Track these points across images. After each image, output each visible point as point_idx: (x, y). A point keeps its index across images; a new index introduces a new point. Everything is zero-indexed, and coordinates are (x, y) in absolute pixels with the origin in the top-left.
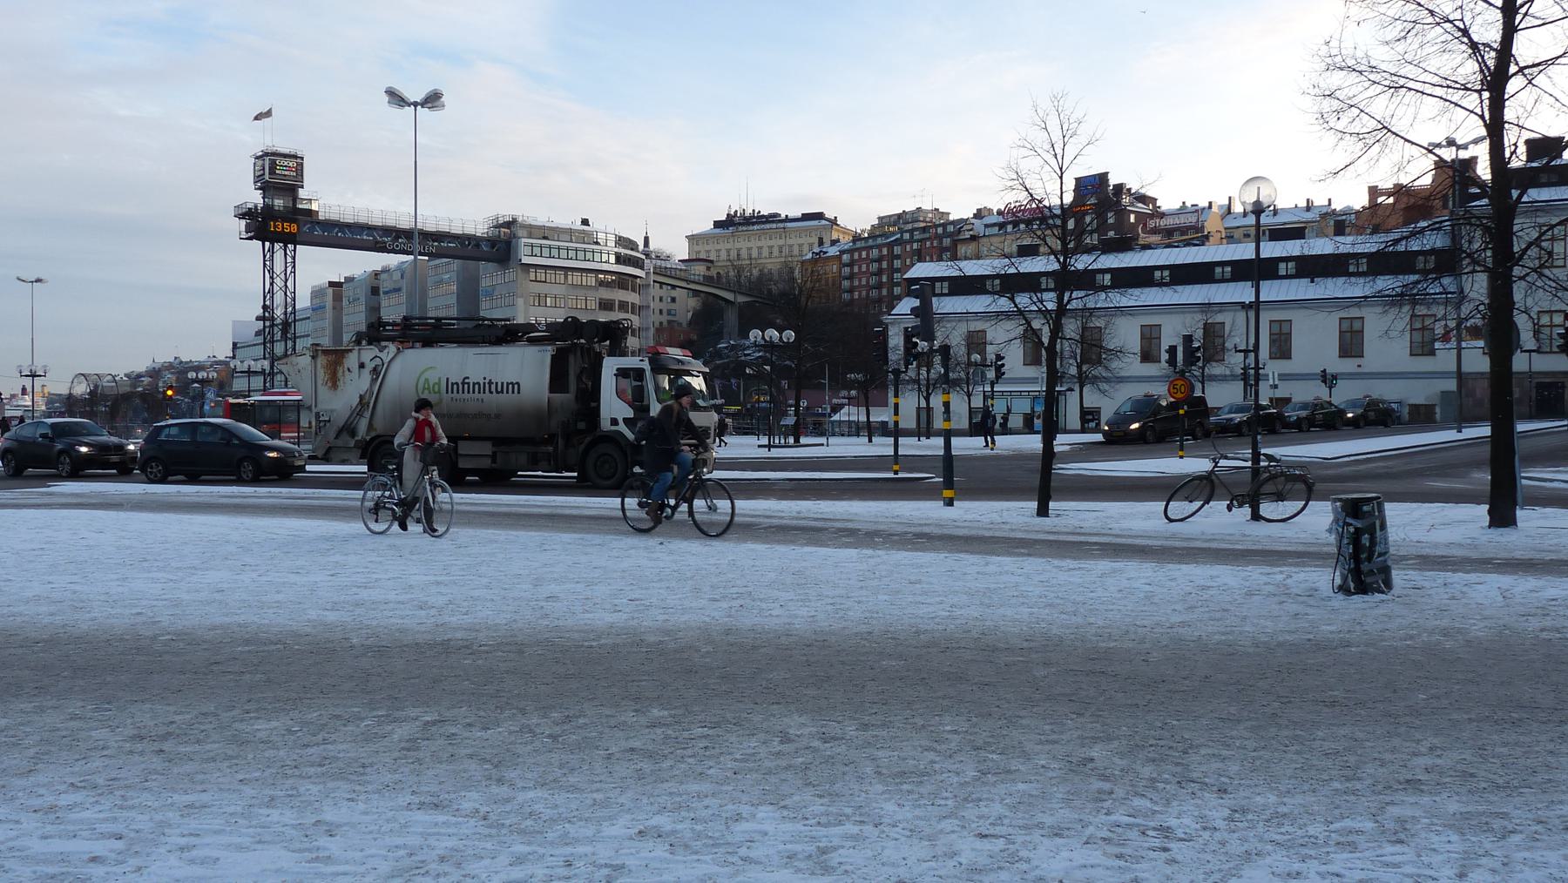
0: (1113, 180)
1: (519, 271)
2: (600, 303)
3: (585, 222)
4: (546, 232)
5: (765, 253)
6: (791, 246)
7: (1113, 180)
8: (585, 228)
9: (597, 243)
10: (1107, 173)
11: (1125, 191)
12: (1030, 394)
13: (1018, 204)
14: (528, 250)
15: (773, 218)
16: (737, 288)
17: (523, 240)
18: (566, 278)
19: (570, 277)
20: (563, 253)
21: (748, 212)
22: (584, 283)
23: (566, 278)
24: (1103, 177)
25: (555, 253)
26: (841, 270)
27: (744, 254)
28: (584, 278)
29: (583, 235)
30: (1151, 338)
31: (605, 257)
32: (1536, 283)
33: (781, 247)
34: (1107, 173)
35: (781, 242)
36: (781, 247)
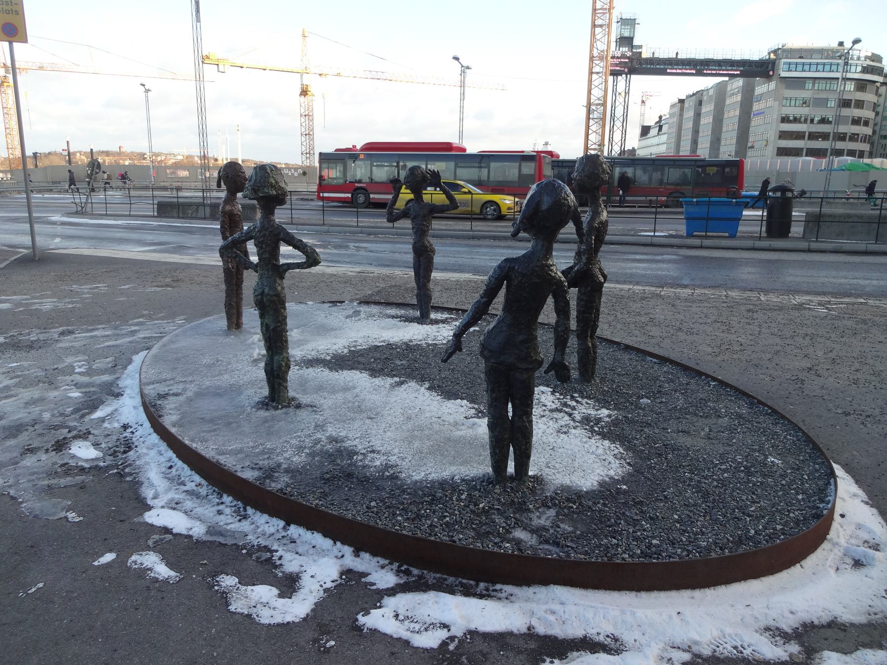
4: (802, 53)
18: (813, 85)
22: (828, 88)
23: (813, 85)
32: (810, 88)
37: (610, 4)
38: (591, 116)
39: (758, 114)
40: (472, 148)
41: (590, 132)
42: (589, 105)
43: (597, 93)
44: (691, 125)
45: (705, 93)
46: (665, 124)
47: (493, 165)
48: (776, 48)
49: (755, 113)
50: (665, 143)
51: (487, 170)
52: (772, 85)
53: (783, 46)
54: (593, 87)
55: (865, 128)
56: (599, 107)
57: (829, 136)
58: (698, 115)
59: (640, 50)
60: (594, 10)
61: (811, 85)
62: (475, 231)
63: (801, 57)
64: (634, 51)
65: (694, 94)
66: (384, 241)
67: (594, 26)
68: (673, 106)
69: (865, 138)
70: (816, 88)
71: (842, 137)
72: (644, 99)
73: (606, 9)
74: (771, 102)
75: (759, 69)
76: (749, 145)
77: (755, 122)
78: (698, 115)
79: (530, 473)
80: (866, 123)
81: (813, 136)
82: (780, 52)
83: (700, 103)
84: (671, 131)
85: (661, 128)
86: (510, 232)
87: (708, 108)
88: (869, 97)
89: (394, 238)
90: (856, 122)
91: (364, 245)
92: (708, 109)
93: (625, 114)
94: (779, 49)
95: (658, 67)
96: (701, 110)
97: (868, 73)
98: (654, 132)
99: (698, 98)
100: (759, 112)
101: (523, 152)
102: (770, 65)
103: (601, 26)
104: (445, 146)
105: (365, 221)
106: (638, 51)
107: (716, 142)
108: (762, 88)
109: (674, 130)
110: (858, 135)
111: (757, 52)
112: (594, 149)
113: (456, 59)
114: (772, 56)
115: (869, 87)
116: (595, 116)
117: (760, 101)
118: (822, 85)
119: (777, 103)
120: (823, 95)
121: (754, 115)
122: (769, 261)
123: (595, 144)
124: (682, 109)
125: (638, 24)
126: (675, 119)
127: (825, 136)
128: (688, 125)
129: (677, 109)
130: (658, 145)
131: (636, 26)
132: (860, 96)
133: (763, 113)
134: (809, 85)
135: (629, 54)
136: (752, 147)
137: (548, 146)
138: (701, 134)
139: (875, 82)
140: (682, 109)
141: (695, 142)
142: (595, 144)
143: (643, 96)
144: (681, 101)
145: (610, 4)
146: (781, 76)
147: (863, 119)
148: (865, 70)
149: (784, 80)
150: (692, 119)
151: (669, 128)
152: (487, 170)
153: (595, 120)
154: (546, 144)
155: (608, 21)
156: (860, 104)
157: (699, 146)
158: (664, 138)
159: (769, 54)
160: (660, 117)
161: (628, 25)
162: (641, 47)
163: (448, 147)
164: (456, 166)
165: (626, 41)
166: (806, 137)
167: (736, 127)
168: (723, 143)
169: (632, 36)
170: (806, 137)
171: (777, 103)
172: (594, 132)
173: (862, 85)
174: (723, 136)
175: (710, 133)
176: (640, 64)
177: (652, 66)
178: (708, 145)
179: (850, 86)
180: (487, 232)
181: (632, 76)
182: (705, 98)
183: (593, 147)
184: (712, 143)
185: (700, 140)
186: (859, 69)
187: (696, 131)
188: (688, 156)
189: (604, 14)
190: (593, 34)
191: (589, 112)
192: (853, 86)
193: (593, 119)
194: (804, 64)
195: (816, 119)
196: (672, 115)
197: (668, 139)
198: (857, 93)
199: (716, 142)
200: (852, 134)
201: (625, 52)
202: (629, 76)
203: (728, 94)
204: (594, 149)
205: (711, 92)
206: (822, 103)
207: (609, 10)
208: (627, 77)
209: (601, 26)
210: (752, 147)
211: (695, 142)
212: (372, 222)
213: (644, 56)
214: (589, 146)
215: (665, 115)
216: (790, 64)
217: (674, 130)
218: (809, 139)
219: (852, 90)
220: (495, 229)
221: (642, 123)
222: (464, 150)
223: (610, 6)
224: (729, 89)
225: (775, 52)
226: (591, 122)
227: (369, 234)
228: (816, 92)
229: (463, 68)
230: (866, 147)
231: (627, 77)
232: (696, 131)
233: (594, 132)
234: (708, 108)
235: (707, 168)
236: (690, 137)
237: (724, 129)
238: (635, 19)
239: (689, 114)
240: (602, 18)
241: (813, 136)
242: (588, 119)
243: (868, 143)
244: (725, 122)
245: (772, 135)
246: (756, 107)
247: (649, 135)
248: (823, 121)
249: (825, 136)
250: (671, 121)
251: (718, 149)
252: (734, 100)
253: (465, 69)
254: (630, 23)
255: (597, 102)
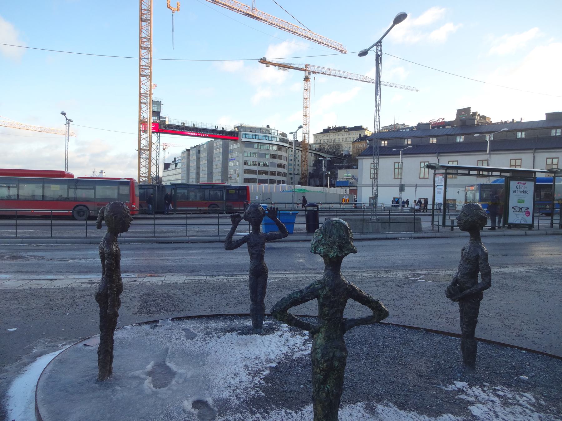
0: (472, 111)
1: (241, 144)
2: (271, 156)
3: (268, 126)
4: (251, 129)
5: (344, 140)
6: (350, 138)
7: (472, 111)
8: (268, 128)
9: (270, 134)
10: (470, 107)
11: (477, 115)
12: (503, 174)
13: (434, 121)
14: (244, 136)
15: (344, 128)
16: (328, 153)
17: (242, 132)
18: (258, 146)
19: (259, 146)
20: (257, 137)
21: (337, 126)
22: (265, 148)
23: (258, 146)
24: (468, 110)
25: (260, 137)
26: (366, 145)
27: (337, 140)
28: (265, 147)
29: (267, 130)
30: (389, 223)
31: (275, 139)
32: (257, 148)
33: (346, 138)
34: (470, 107)
35: (346, 137)
36: (346, 138)
37: (150, 92)
38: (141, 156)
39: (232, 160)
40: (77, 174)
41: (141, 166)
42: (140, 150)
43: (144, 143)
44: (195, 164)
45: (201, 147)
46: (180, 162)
47: (98, 187)
48: (238, 125)
49: (230, 159)
50: (180, 174)
51: (93, 191)
52: (238, 145)
53: (241, 125)
54: (142, 139)
55: (283, 169)
56: (146, 151)
57: (268, 173)
58: (198, 159)
59: (165, 120)
60: (140, 94)
61: (257, 146)
62: (189, 236)
63: (251, 132)
64: (161, 119)
65: (195, 147)
66: (51, 249)
67: (140, 103)
68: (183, 153)
69: (284, 174)
70: (259, 148)
71: (273, 173)
72: (164, 147)
73: (147, 94)
74: (238, 154)
75: (230, 136)
76: (229, 176)
77: (231, 164)
78: (198, 159)
79: (310, 408)
80: (284, 167)
81: (261, 173)
82: (240, 128)
83: (199, 152)
84: (184, 167)
85: (176, 165)
86: (225, 236)
87: (204, 155)
88: (283, 153)
89: (54, 246)
90: (279, 166)
91: (36, 254)
92: (204, 155)
93: (158, 156)
94: (239, 126)
95: (175, 130)
96: (200, 156)
97: (282, 142)
98: (172, 167)
99: (198, 149)
100: (233, 158)
101: (119, 179)
102: (236, 134)
103: (145, 103)
104: (59, 173)
105: (23, 232)
106: (163, 120)
107: (210, 174)
108: (233, 146)
109: (185, 166)
110: (281, 172)
111: (229, 125)
112: (145, 177)
113: (64, 114)
114: (236, 130)
115: (283, 148)
116: (144, 157)
117: (232, 153)
118: (262, 147)
119: (241, 154)
120: (263, 152)
121: (230, 160)
122: (504, 244)
123: (145, 173)
124: (189, 155)
125: (162, 105)
126: (185, 160)
127: (266, 173)
128: (193, 164)
129: (186, 155)
130: (175, 175)
131: (161, 106)
132: (279, 153)
133: (235, 159)
134: (256, 146)
135: (158, 121)
136: (230, 177)
137: (104, 174)
138: (201, 170)
139: (285, 147)
140: (189, 155)
141: (198, 174)
142: (145, 173)
143: (163, 146)
144: (188, 150)
145: (150, 92)
146: (242, 140)
147: (282, 165)
148: (281, 140)
149: (243, 142)
150: (195, 160)
151: (182, 165)
152: (93, 191)
153: (145, 159)
154: (102, 172)
155: (149, 101)
156: (280, 157)
157: (201, 176)
158: (179, 171)
159: (235, 128)
160: (175, 159)
161: (156, 105)
162: (165, 118)
163: (61, 174)
164: (69, 188)
165: (156, 114)
166: (257, 173)
167: (221, 166)
168: (214, 175)
169: (159, 111)
170: (257, 173)
171: (241, 154)
172: (144, 166)
173: (280, 148)
174: (214, 171)
175: (206, 169)
176: (165, 127)
177: (172, 129)
178: (206, 176)
179: (275, 148)
180: (203, 236)
181: (160, 134)
182: (202, 149)
183: (144, 175)
184: (208, 174)
185: (201, 173)
186: (278, 140)
187: (198, 168)
188: (221, 184)
189: (146, 97)
190: (140, 108)
191: (140, 154)
192: (276, 148)
193: (143, 158)
194: (252, 135)
195: (261, 164)
196: (183, 158)
197: (182, 171)
198: (278, 151)
199: (210, 174)
200: (279, 172)
201: (156, 120)
202: (158, 134)
203: (215, 148)
204: (145, 177)
205: (205, 146)
206: (262, 155)
207: (150, 94)
208: (157, 134)
209: (145, 103)
210: (230, 177)
211: (198, 174)
212: (25, 233)
213: (167, 123)
214: (141, 174)
215: (178, 158)
216: (246, 134)
217: (185, 166)
218: (259, 174)
219: (276, 150)
220: (141, 235)
221: (164, 161)
222: (72, 176)
223: (150, 93)
224: (215, 145)
225: (238, 127)
226: (142, 160)
227: (30, 244)
228: (260, 150)
229: (67, 121)
230: (284, 179)
231: (157, 134)
232: (198, 168)
233: (144, 166)
234: (204, 155)
235: (230, 190)
236: (195, 171)
237: (214, 167)
238: (160, 102)
239: (193, 158)
240: (145, 99)
241: (261, 173)
242: (140, 158)
243: (286, 177)
244: (214, 163)
245: (240, 171)
246: (231, 156)
247: (169, 169)
248: (265, 165)
249: (266, 173)
250: (183, 161)
251: (212, 178)
252: (218, 153)
253: (69, 121)
254: (158, 103)
255: (145, 148)
